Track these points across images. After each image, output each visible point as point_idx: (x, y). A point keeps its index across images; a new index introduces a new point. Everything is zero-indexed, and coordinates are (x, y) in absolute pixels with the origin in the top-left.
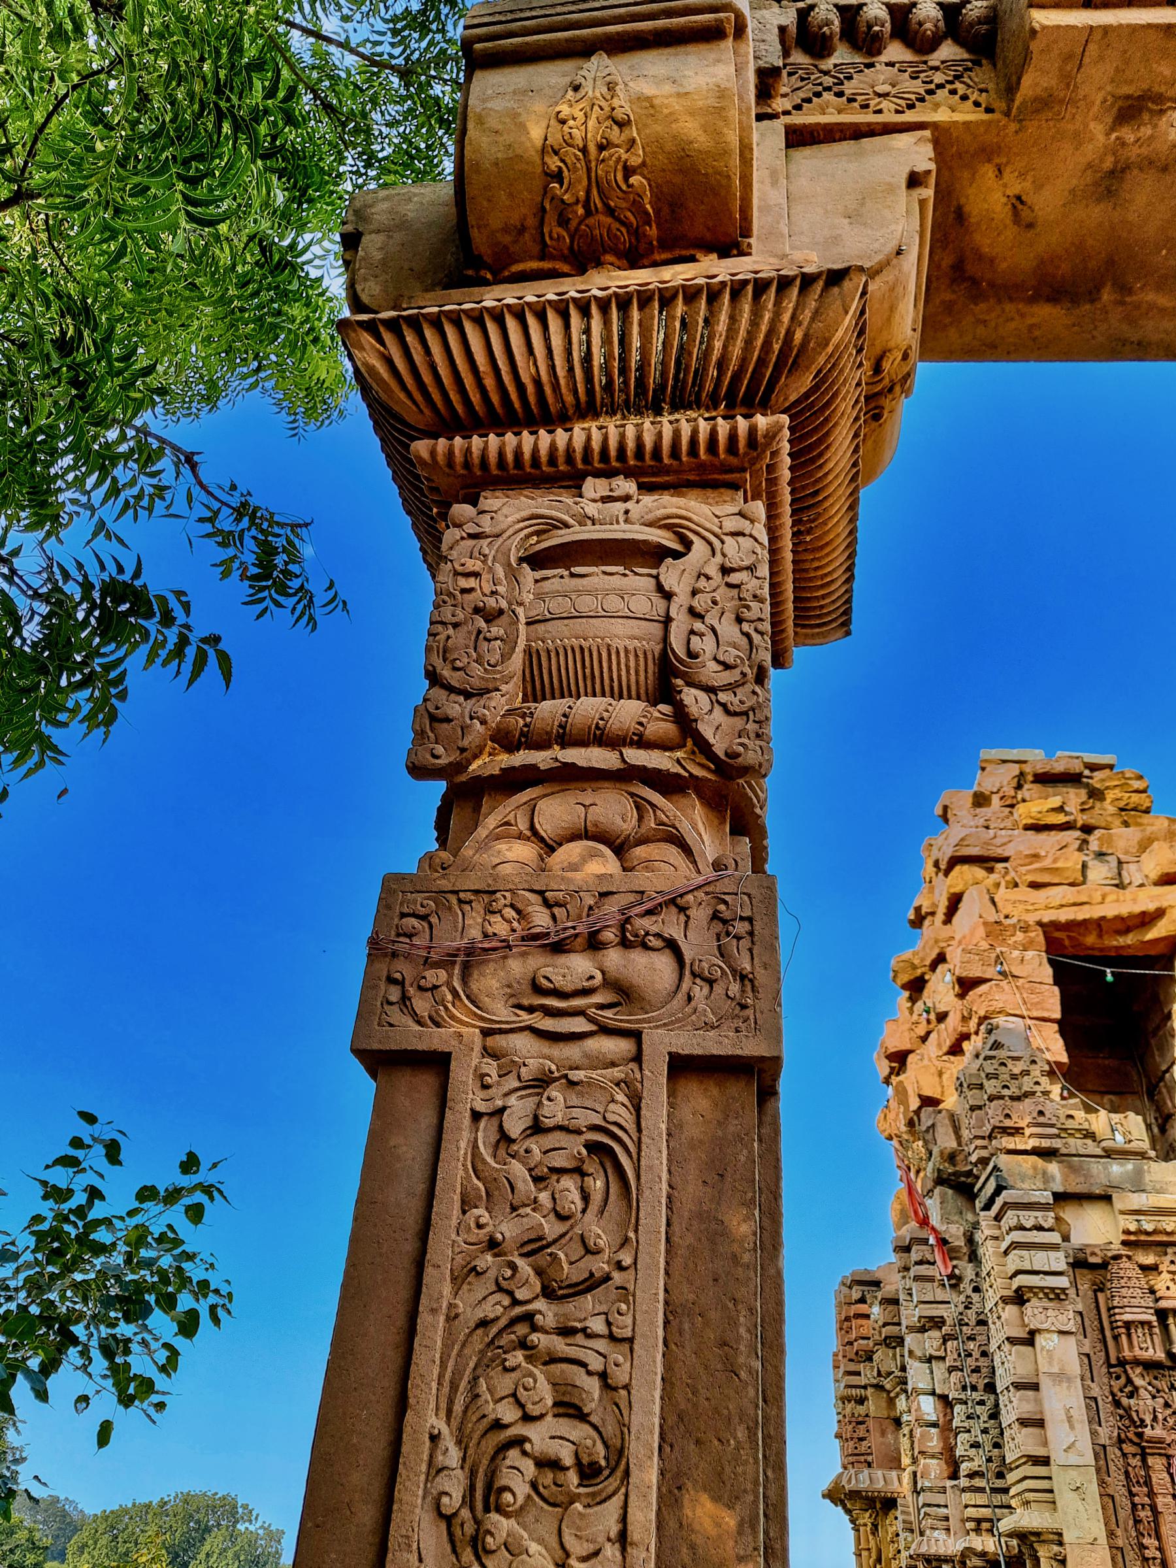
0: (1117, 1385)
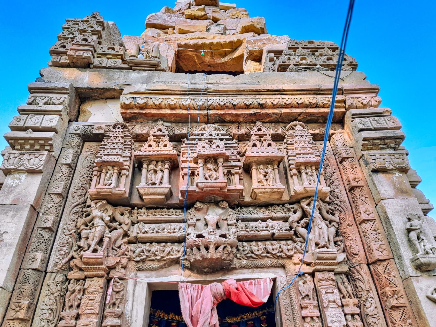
0: (81, 221)
